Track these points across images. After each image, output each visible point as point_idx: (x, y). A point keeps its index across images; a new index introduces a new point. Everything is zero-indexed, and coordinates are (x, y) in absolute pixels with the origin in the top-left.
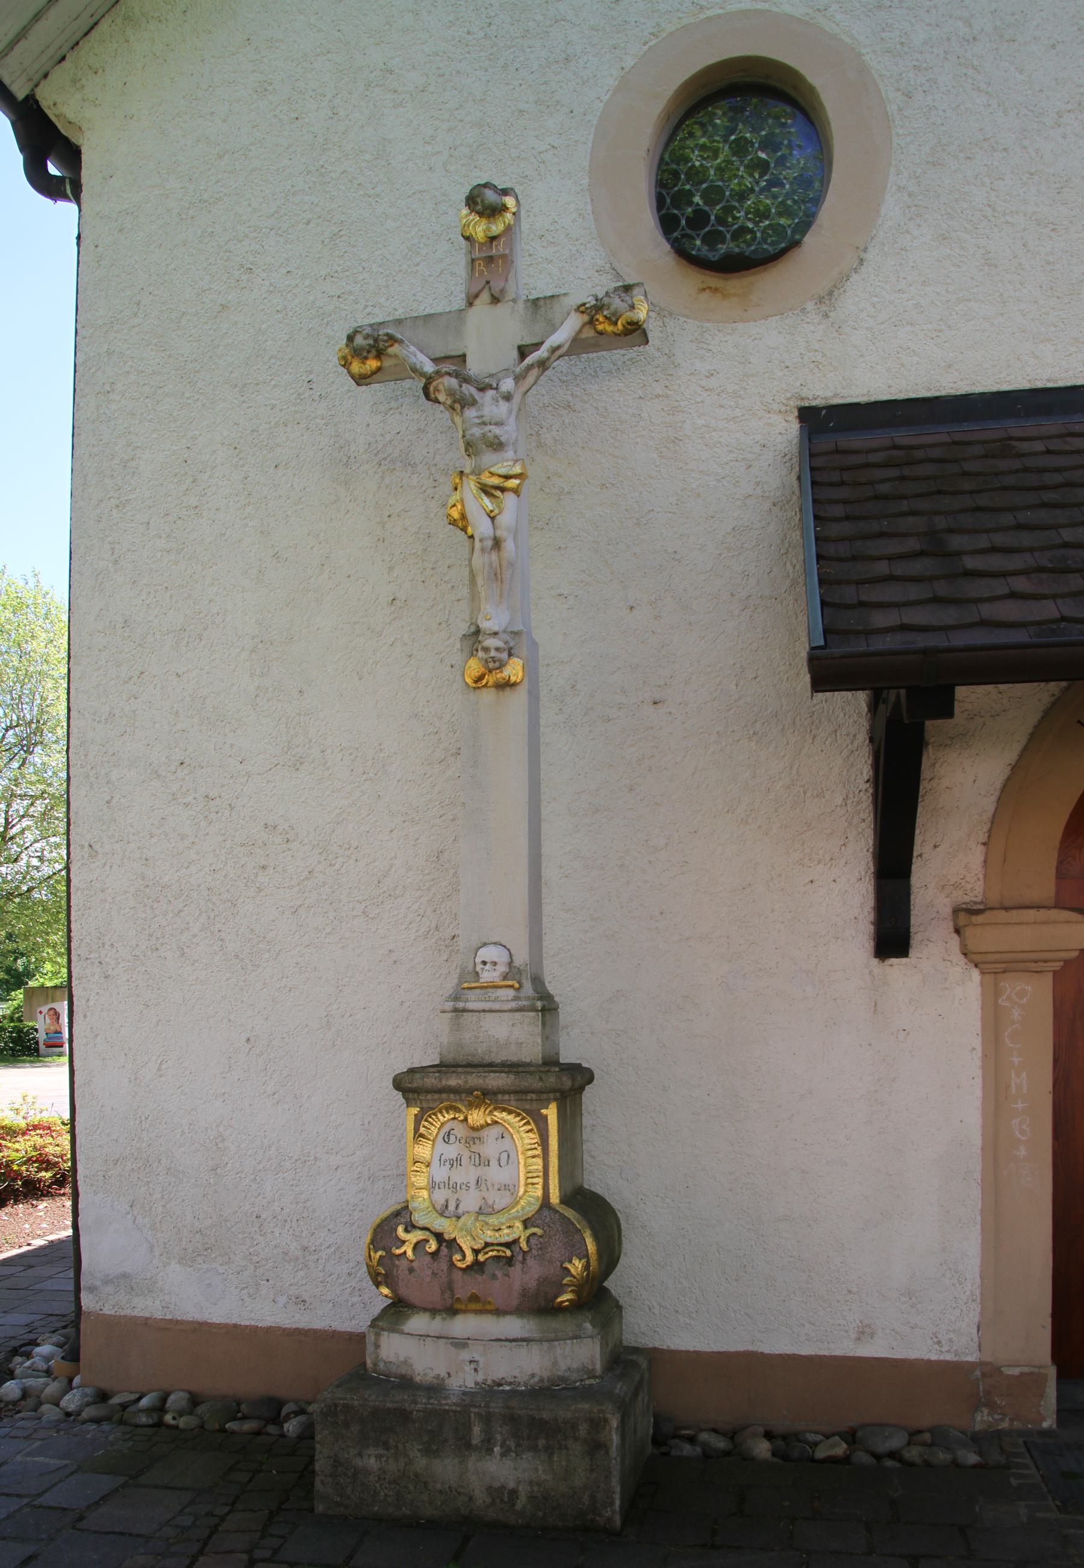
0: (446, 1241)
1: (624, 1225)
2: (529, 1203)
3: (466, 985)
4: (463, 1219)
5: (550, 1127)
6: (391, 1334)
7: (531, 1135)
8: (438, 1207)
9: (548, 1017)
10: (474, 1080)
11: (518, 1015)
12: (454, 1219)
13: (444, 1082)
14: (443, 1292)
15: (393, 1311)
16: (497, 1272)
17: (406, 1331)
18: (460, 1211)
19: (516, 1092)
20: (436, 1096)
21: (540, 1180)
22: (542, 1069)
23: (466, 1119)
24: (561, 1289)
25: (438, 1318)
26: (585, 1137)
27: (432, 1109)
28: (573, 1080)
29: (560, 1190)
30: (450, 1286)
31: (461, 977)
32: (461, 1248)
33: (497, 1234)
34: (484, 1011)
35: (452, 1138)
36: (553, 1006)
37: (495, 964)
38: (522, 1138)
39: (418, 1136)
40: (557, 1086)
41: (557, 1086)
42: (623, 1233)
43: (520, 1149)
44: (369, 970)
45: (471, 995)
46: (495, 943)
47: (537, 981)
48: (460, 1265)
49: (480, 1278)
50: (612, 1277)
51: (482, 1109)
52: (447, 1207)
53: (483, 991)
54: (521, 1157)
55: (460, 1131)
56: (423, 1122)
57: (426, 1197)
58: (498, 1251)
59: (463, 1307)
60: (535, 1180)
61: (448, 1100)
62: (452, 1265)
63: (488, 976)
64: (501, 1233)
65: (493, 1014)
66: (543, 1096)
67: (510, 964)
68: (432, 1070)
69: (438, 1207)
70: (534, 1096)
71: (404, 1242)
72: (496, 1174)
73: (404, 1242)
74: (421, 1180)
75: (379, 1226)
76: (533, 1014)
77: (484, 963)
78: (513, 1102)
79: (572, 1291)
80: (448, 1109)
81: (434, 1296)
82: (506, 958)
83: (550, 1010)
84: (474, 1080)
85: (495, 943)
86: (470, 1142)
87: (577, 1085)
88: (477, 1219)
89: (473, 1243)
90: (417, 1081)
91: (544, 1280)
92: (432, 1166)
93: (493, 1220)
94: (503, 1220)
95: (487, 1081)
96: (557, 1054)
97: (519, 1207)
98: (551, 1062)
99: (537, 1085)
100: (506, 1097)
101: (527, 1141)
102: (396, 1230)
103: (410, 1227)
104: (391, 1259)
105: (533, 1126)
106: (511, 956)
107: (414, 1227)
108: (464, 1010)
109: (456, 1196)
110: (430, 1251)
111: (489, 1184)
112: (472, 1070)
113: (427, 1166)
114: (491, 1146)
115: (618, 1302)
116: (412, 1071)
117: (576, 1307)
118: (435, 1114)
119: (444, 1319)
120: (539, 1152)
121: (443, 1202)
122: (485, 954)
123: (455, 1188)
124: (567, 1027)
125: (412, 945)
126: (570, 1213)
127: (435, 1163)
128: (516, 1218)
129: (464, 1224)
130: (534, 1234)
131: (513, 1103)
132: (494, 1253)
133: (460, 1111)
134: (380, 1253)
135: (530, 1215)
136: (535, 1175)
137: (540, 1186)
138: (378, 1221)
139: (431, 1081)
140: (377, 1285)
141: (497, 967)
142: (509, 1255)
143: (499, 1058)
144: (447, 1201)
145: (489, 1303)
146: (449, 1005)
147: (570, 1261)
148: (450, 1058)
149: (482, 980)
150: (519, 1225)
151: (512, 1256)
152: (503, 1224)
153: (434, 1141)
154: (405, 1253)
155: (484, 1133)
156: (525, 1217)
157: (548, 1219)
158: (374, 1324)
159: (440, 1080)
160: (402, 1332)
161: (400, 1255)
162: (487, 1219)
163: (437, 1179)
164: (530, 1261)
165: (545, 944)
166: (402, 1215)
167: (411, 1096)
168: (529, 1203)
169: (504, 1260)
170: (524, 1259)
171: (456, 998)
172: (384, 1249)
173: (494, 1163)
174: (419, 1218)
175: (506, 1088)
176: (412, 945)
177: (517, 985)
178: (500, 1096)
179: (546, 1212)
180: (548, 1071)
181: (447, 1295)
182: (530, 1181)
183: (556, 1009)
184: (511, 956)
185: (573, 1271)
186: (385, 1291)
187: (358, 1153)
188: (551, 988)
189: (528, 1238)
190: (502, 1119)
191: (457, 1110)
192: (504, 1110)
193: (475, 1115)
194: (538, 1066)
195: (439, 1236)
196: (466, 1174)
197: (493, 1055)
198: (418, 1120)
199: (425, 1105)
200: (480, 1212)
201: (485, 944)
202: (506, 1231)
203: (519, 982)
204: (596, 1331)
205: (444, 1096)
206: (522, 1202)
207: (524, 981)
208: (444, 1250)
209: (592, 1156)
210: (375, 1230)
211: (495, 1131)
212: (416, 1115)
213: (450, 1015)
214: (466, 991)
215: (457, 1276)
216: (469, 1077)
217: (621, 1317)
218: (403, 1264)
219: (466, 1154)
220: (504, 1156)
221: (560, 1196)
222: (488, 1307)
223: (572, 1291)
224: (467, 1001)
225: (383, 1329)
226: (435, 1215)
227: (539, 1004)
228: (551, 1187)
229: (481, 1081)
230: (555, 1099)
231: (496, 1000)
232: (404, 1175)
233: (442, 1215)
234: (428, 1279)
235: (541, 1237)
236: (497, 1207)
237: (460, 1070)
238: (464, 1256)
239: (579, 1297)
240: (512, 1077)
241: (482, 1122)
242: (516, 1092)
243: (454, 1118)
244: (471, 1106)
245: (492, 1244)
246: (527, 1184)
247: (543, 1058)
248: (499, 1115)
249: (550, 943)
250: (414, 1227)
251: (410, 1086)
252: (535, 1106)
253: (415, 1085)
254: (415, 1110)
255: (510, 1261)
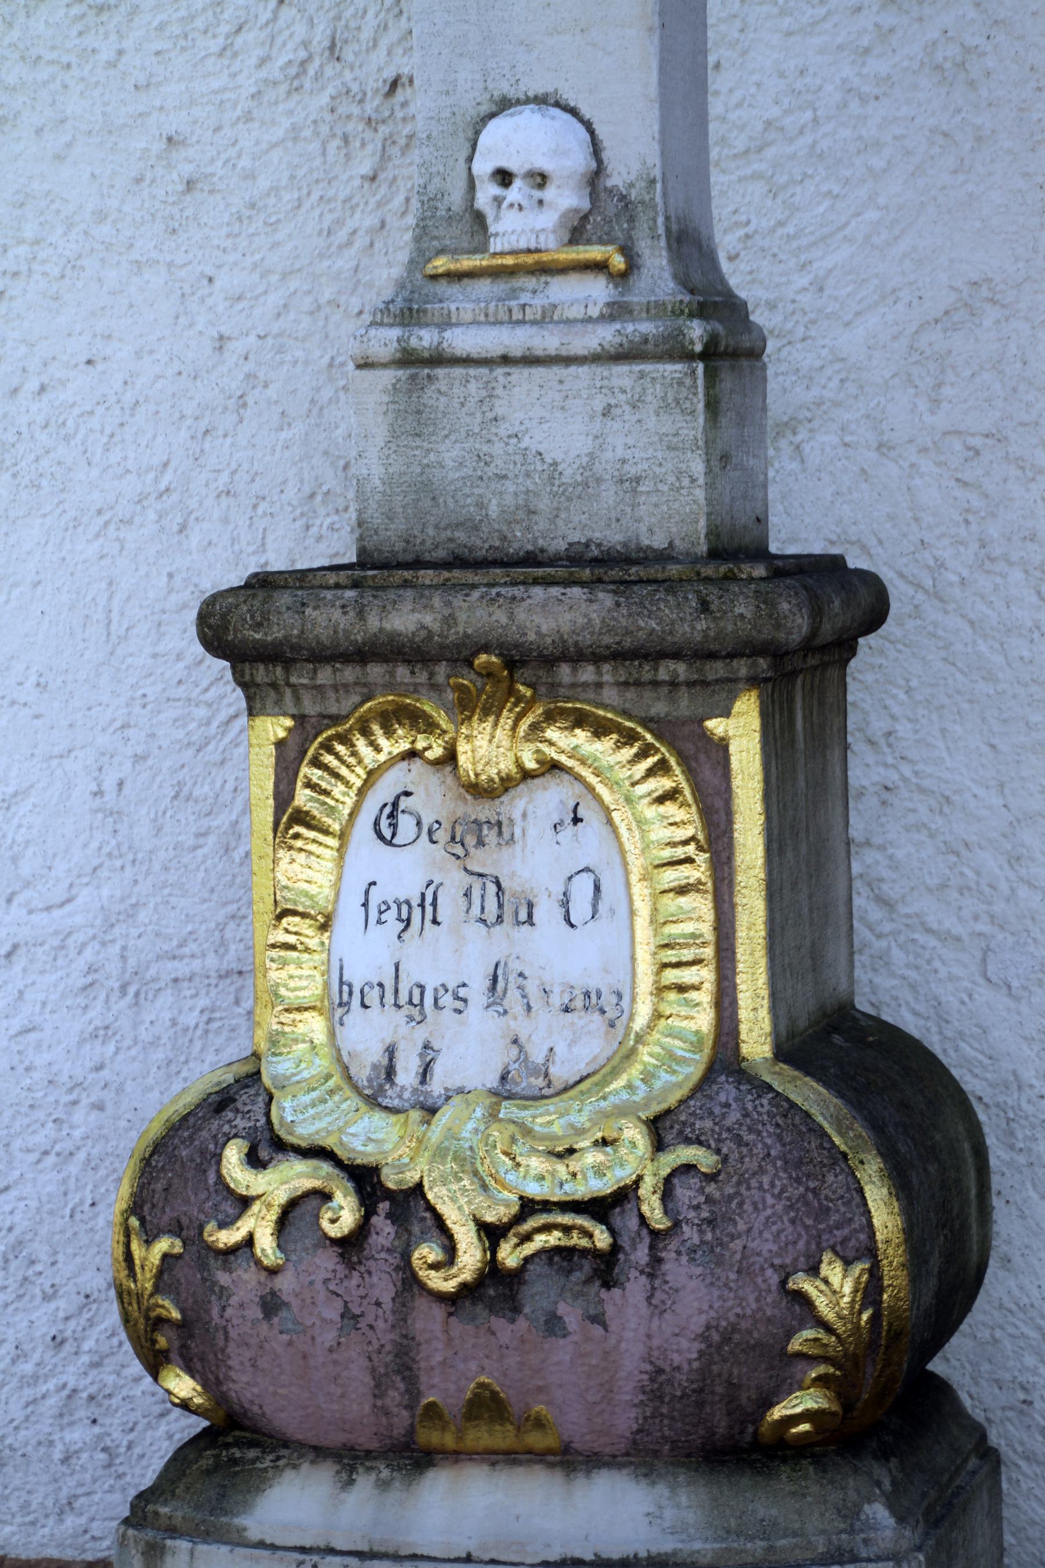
0: (389, 1195)
1: (997, 1155)
2: (670, 1058)
3: (441, 264)
4: (444, 1118)
5: (737, 782)
6: (202, 1548)
7: (670, 809)
8: (362, 1074)
9: (727, 382)
10: (476, 613)
11: (622, 374)
12: (415, 1115)
13: (373, 622)
14: (379, 1388)
15: (207, 1461)
16: (562, 1309)
17: (254, 1534)
18: (436, 1087)
19: (618, 656)
20: (349, 673)
21: (706, 975)
22: (708, 571)
23: (450, 757)
24: (781, 1371)
25: (365, 1483)
26: (857, 828)
27: (336, 719)
28: (817, 613)
29: (774, 1010)
30: (404, 1363)
31: (422, 231)
32: (439, 1221)
33: (561, 1169)
34: (506, 360)
35: (406, 825)
36: (746, 342)
37: (540, 179)
38: (641, 822)
39: (290, 819)
40: (756, 638)
41: (756, 638)
42: (996, 1182)
43: (636, 865)
44: (101, 216)
45: (461, 300)
46: (541, 101)
47: (690, 244)
48: (436, 1281)
49: (505, 1331)
50: (958, 1343)
51: (506, 720)
52: (390, 1072)
53: (501, 287)
54: (640, 892)
55: (431, 798)
56: (306, 771)
57: (320, 1036)
58: (567, 1229)
59: (449, 1440)
60: (688, 975)
61: (390, 687)
62: (410, 1282)
63: (522, 226)
64: (574, 1164)
65: (539, 372)
66: (713, 666)
67: (595, 179)
68: (332, 578)
69: (362, 1074)
70: (681, 669)
71: (245, 1202)
72: (554, 955)
73: (245, 1202)
74: (301, 979)
75: (158, 1147)
76: (674, 369)
77: (504, 177)
78: (606, 688)
79: (822, 1381)
80: (389, 719)
81: (345, 1395)
82: (576, 159)
83: (734, 354)
84: (476, 613)
85: (541, 101)
86: (464, 837)
87: (828, 630)
88: (493, 1116)
89: (480, 1199)
90: (284, 623)
91: (726, 1339)
92: (337, 925)
93: (549, 1120)
94: (581, 1119)
95: (521, 616)
96: (761, 520)
97: (634, 1072)
98: (735, 550)
99: (692, 628)
100: (587, 674)
101: (661, 833)
102: (218, 1158)
103: (268, 1147)
104: (203, 1266)
105: (678, 778)
106: (596, 149)
107: (280, 1146)
108: (439, 359)
109: (421, 1034)
110: (334, 1231)
111: (532, 988)
112: (470, 576)
113: (324, 927)
114: (536, 854)
115: (983, 1437)
116: (263, 583)
117: (837, 1442)
118: (344, 739)
119: (384, 1485)
120: (699, 872)
121: (376, 1055)
122: (519, 139)
123: (416, 1004)
124: (791, 425)
125: (248, 117)
126: (807, 1093)
127: (349, 914)
128: (622, 1111)
129: (451, 1135)
130: (688, 1168)
131: (610, 695)
132: (553, 1239)
133: (430, 727)
134: (163, 1245)
135: (672, 1100)
136: (687, 955)
137: (705, 997)
138: (156, 1130)
139: (329, 619)
140: (155, 1363)
141: (549, 193)
142: (597, 1248)
143: (565, 530)
144: (391, 1051)
145: (539, 1424)
146: (385, 341)
147: (814, 1270)
148: (391, 535)
149: (496, 245)
150: (635, 1135)
151: (615, 1248)
152: (580, 1132)
153: (343, 836)
154: (249, 1241)
155: (516, 805)
156: (656, 1108)
157: (734, 1116)
158: (141, 1512)
159: (361, 615)
160: (238, 1540)
161: (232, 1251)
162: (525, 1115)
163: (357, 976)
164: (677, 1270)
165: (716, 107)
166: (239, 1104)
167: (261, 674)
168: (670, 1058)
169: (587, 1266)
170: (656, 1260)
171: (409, 315)
172: (177, 1229)
173: (547, 912)
174: (299, 1116)
175: (586, 639)
176: (248, 117)
177: (618, 262)
178: (564, 672)
179: (726, 1091)
180: (731, 577)
181: (394, 1396)
182: (671, 976)
183: (755, 353)
184: (596, 149)
185: (822, 1304)
186: (182, 1385)
187: (84, 896)
188: (738, 278)
189: (668, 1180)
190: (574, 753)
191: (425, 724)
192: (580, 720)
193: (482, 742)
194: (696, 560)
195: (364, 1178)
196: (453, 954)
197: (541, 524)
198: (288, 760)
199: (310, 708)
200: (504, 1091)
201: (504, 105)
202: (592, 1158)
203: (627, 251)
204: (910, 1536)
205: (376, 671)
206: (646, 1056)
207: (643, 246)
208: (384, 1230)
209: (886, 903)
210: (146, 1162)
211: (549, 799)
212: (280, 744)
213: (387, 377)
214: (442, 288)
215: (429, 1320)
216: (458, 601)
217: (996, 1495)
218: (243, 1283)
219: (453, 881)
220: (583, 887)
221: (776, 1033)
222: (536, 1440)
223: (822, 1381)
224: (446, 323)
225: (173, 1531)
226: (355, 1101)
227: (696, 332)
228: (744, 999)
229: (501, 616)
230: (754, 682)
231: (546, 318)
232: (242, 973)
233: (373, 1101)
234: (329, 1337)
235: (711, 1178)
236: (562, 1072)
237: (427, 576)
238: (451, 1249)
239: (847, 1406)
240: (606, 599)
241: (506, 766)
242: (618, 656)
243: (412, 754)
244: (466, 707)
245: (546, 1206)
246: (660, 990)
247: (713, 532)
248: (564, 741)
249: (738, 100)
250: (280, 1146)
251: (252, 636)
252: (685, 705)
253: (276, 634)
254: (276, 727)
255: (605, 1267)
